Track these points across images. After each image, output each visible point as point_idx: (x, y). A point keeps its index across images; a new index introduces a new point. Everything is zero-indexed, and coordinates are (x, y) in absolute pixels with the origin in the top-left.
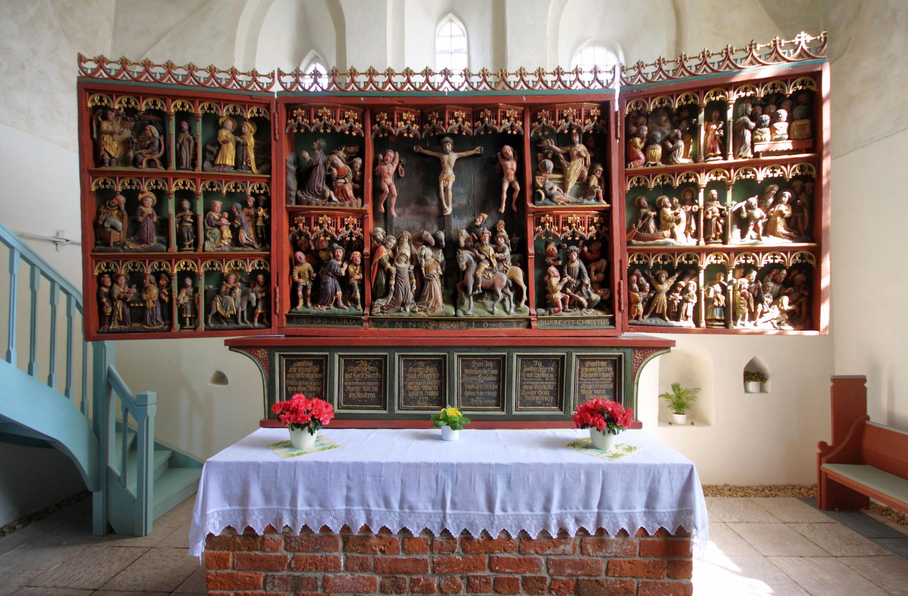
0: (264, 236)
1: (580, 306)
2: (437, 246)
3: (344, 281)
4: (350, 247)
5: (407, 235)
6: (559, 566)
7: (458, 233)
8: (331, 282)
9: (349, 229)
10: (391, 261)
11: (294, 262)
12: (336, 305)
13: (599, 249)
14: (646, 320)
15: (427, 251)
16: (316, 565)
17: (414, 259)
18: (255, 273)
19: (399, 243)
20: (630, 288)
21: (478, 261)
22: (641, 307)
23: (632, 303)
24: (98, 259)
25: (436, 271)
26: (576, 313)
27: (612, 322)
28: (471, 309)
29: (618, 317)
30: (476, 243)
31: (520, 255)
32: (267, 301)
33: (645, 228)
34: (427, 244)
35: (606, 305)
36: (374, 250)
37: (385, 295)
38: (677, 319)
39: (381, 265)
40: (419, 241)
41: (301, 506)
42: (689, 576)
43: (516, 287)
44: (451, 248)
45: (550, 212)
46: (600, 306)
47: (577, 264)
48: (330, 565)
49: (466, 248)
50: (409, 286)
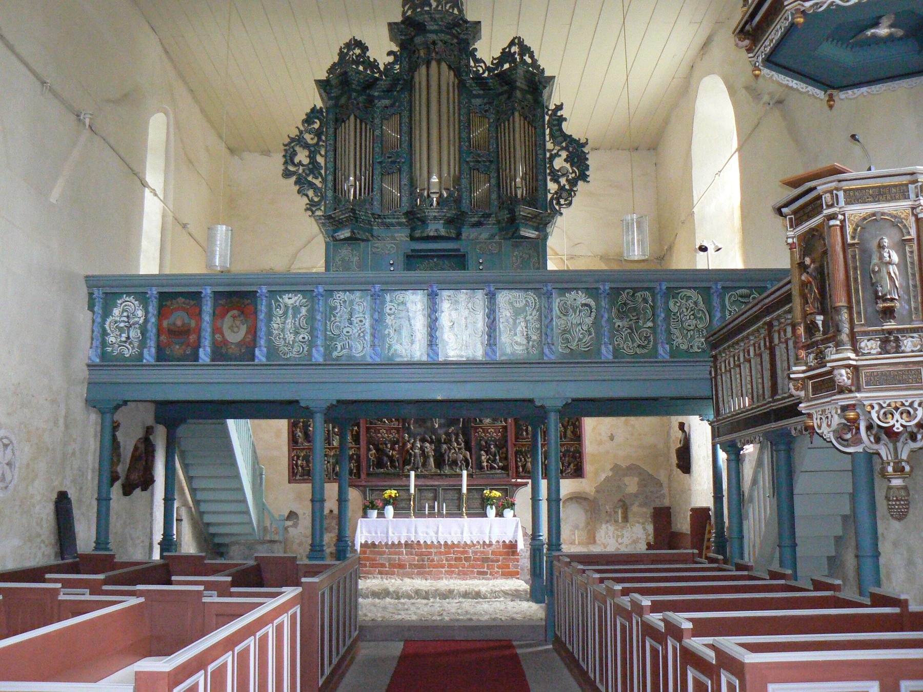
0: (356, 439)
1: (495, 468)
2: (431, 442)
3: (391, 459)
4: (394, 443)
5: (418, 437)
6: (475, 553)
7: (441, 436)
8: (385, 459)
9: (394, 435)
10: (412, 449)
11: (369, 450)
12: (387, 468)
13: (502, 444)
14: (523, 474)
15: (427, 445)
16: (395, 553)
17: (422, 449)
18: (353, 455)
19: (415, 442)
20: (516, 461)
21: (450, 449)
22: (521, 469)
23: (517, 467)
24: (293, 449)
25: (432, 453)
26: (493, 472)
27: (508, 475)
28: (447, 470)
29: (510, 472)
30: (448, 442)
31: (468, 447)
32: (358, 467)
33: (522, 434)
34: (427, 441)
35: (505, 468)
36: (404, 444)
37: (408, 464)
38: (845, 425)
39: (408, 451)
40: (423, 440)
41: (390, 534)
42: (469, 515)
43: (466, 461)
44: (438, 443)
45: (481, 427)
46: (502, 468)
47: (493, 449)
48: (401, 553)
49: (445, 443)
50: (420, 460)
